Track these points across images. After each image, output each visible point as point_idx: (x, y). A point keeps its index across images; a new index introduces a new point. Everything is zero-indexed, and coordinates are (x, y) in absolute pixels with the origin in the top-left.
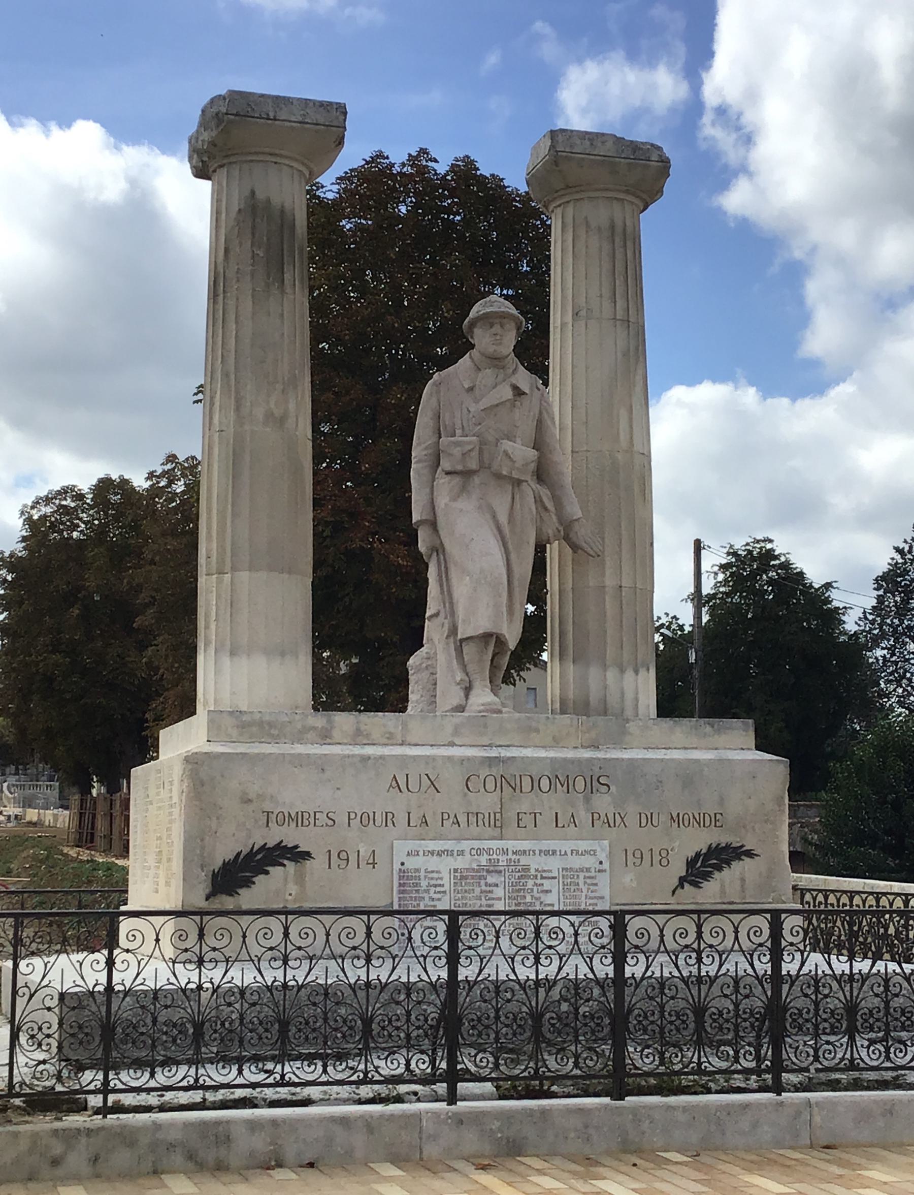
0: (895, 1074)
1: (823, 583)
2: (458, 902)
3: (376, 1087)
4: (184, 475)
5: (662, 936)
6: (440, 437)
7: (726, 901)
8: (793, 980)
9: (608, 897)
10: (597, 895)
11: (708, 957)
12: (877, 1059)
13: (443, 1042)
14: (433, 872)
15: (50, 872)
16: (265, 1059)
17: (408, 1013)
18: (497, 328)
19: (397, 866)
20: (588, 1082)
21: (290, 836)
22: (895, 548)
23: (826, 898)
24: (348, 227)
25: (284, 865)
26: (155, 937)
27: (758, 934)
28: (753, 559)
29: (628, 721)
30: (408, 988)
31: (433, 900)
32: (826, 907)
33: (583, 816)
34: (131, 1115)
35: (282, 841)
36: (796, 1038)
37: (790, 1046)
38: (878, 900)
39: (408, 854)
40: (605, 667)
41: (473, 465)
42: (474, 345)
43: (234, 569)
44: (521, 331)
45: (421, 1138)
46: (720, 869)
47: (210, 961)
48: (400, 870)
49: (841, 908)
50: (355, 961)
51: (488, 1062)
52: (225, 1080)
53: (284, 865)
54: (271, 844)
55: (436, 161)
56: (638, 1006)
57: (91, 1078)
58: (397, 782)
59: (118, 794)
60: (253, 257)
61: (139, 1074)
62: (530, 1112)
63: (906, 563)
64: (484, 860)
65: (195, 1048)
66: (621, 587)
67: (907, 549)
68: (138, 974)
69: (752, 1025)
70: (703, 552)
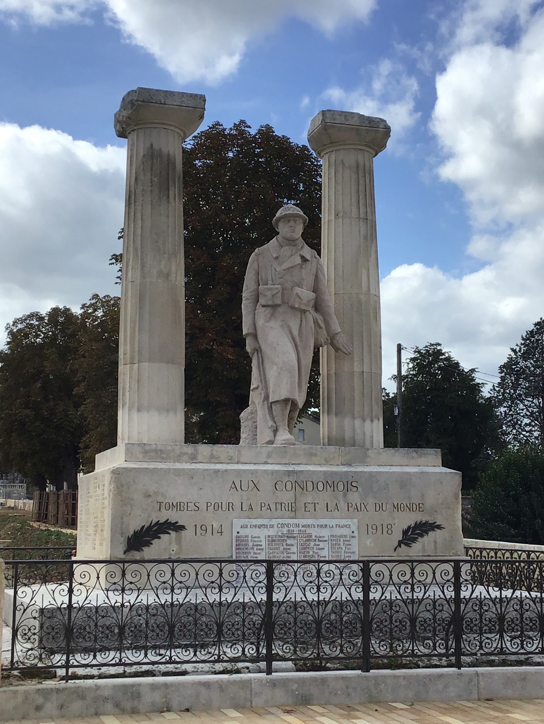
0: (526, 657)
1: (470, 369)
2: (271, 555)
3: (225, 664)
4: (103, 306)
5: (391, 575)
6: (259, 285)
7: (426, 555)
8: (468, 601)
9: (357, 552)
10: (351, 551)
11: (418, 588)
12: (516, 648)
13: (264, 637)
14: (255, 537)
15: (23, 536)
16: (160, 647)
17: (244, 621)
18: (292, 223)
19: (235, 534)
20: (348, 661)
21: (173, 516)
22: (511, 349)
23: (481, 553)
24: (199, 165)
25: (170, 534)
26: (150, 577)
27: (446, 574)
28: (430, 355)
29: (368, 449)
30: (244, 605)
31: (256, 554)
32: (481, 558)
33: (343, 505)
34: (82, 681)
35: (168, 520)
36: (468, 635)
37: (466, 640)
38: (512, 554)
39: (241, 527)
40: (354, 418)
41: (279, 302)
42: (279, 233)
43: (139, 362)
44: (306, 224)
45: (251, 695)
46: (422, 536)
47: (129, 590)
48: (237, 536)
49: (490, 559)
50: (165, 590)
51: (290, 649)
52: (137, 660)
53: (170, 534)
54: (162, 521)
55: (250, 127)
56: (467, 616)
57: (58, 659)
58: (235, 485)
59: (62, 491)
60: (152, 182)
61: (86, 657)
62: (315, 679)
63: (517, 357)
64: (285, 530)
65: (67, 641)
66: (363, 372)
67: (518, 349)
68: (87, 598)
69: (444, 628)
70: (402, 351)
